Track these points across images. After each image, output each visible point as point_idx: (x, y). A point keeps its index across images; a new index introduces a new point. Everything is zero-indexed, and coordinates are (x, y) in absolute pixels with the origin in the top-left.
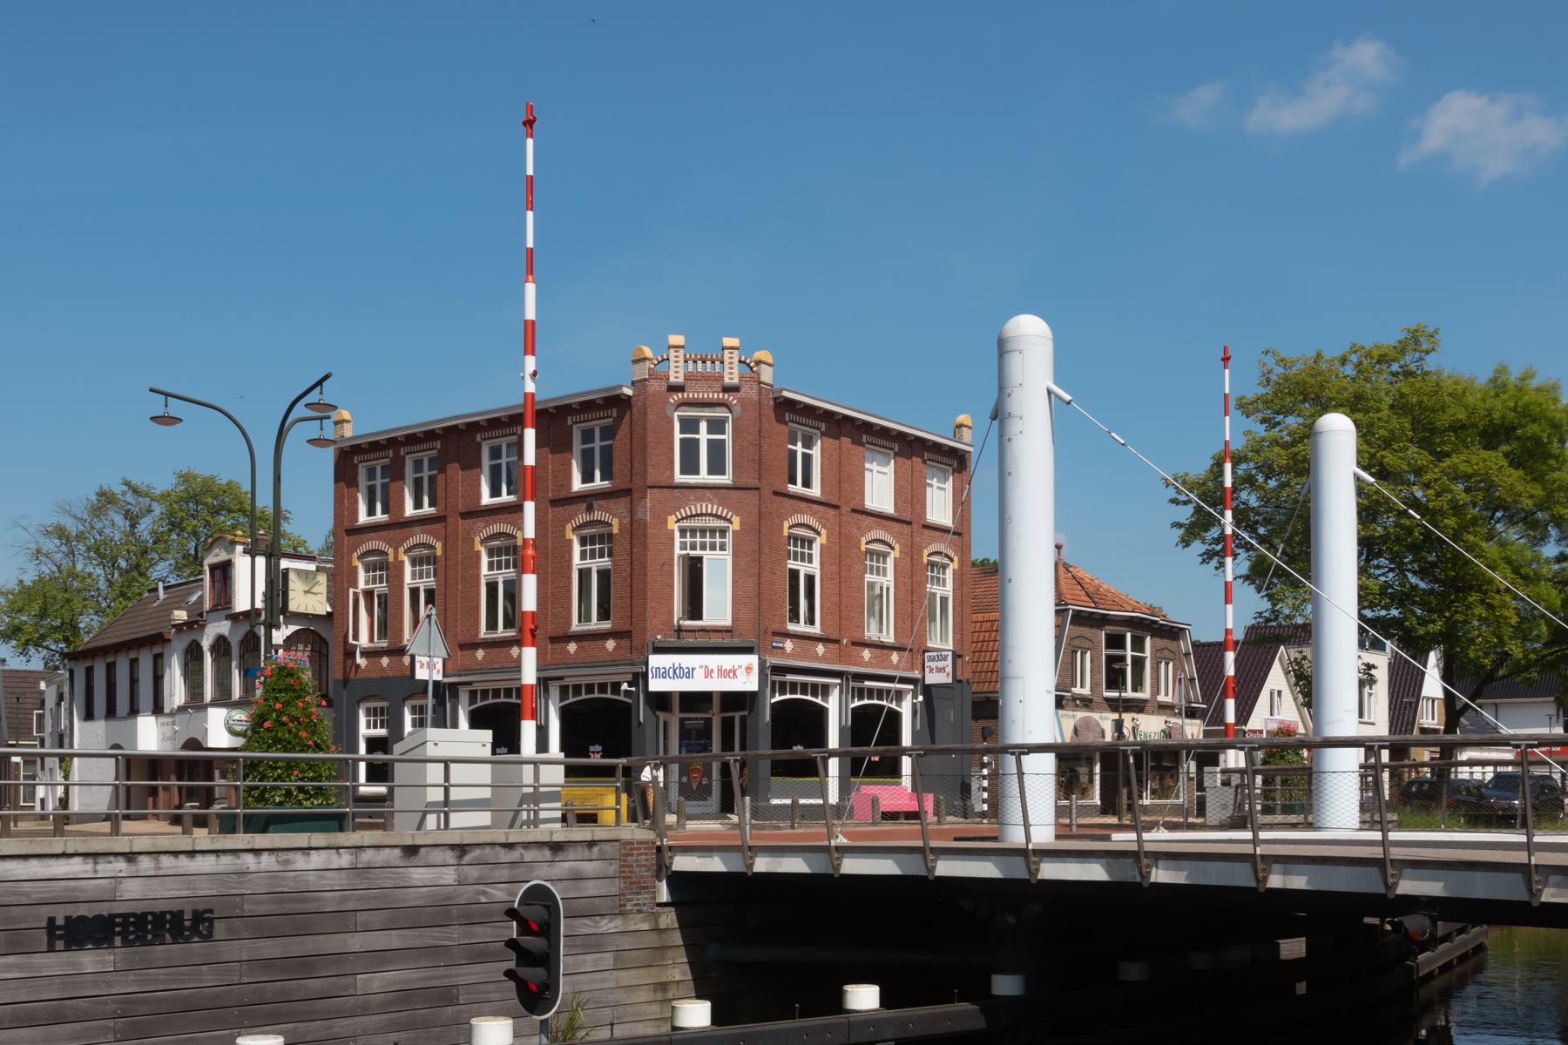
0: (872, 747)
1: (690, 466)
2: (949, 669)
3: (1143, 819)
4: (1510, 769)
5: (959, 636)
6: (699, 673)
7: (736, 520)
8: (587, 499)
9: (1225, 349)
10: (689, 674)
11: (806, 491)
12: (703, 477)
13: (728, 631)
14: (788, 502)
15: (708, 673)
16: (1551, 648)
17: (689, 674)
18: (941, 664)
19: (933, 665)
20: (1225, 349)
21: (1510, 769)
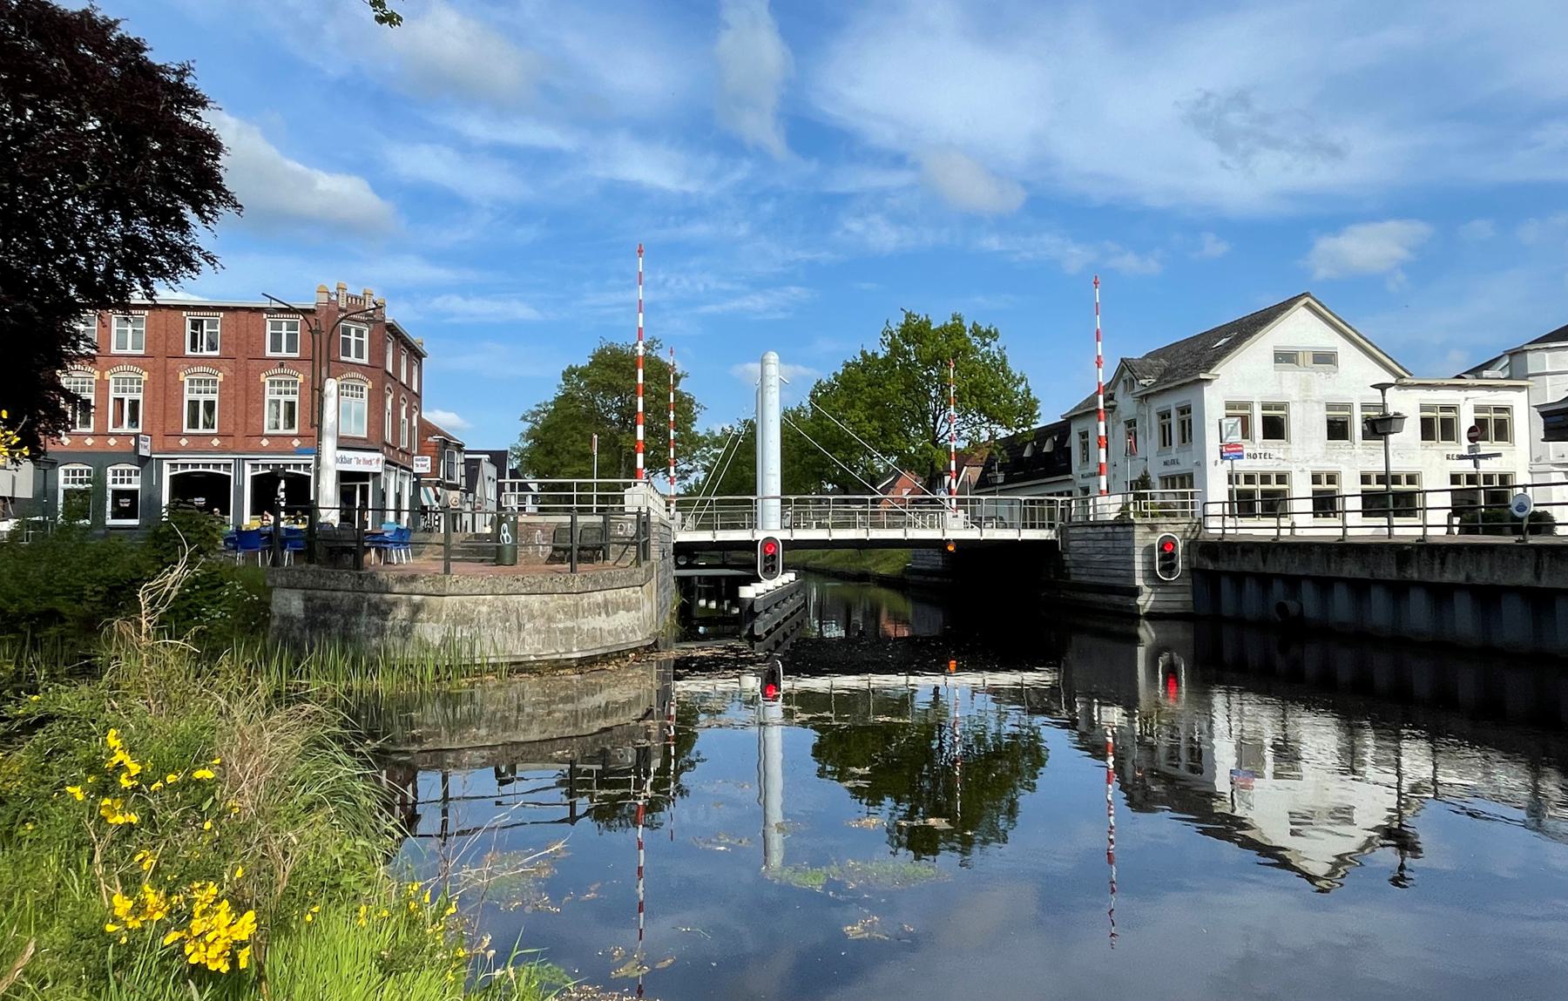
0: (232, 474)
1: (276, 346)
2: (429, 465)
3: (405, 525)
4: (936, 579)
5: (1404, 513)
6: (354, 461)
7: (301, 376)
8: (282, 362)
9: (640, 246)
10: (349, 461)
11: (359, 361)
12: (284, 353)
13: (365, 439)
14: (341, 365)
15: (359, 462)
16: (18, 426)
17: (349, 461)
18: (424, 463)
19: (419, 463)
20: (640, 246)
21: (936, 579)
